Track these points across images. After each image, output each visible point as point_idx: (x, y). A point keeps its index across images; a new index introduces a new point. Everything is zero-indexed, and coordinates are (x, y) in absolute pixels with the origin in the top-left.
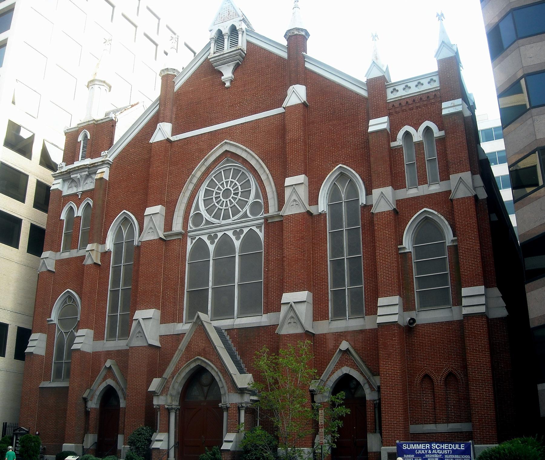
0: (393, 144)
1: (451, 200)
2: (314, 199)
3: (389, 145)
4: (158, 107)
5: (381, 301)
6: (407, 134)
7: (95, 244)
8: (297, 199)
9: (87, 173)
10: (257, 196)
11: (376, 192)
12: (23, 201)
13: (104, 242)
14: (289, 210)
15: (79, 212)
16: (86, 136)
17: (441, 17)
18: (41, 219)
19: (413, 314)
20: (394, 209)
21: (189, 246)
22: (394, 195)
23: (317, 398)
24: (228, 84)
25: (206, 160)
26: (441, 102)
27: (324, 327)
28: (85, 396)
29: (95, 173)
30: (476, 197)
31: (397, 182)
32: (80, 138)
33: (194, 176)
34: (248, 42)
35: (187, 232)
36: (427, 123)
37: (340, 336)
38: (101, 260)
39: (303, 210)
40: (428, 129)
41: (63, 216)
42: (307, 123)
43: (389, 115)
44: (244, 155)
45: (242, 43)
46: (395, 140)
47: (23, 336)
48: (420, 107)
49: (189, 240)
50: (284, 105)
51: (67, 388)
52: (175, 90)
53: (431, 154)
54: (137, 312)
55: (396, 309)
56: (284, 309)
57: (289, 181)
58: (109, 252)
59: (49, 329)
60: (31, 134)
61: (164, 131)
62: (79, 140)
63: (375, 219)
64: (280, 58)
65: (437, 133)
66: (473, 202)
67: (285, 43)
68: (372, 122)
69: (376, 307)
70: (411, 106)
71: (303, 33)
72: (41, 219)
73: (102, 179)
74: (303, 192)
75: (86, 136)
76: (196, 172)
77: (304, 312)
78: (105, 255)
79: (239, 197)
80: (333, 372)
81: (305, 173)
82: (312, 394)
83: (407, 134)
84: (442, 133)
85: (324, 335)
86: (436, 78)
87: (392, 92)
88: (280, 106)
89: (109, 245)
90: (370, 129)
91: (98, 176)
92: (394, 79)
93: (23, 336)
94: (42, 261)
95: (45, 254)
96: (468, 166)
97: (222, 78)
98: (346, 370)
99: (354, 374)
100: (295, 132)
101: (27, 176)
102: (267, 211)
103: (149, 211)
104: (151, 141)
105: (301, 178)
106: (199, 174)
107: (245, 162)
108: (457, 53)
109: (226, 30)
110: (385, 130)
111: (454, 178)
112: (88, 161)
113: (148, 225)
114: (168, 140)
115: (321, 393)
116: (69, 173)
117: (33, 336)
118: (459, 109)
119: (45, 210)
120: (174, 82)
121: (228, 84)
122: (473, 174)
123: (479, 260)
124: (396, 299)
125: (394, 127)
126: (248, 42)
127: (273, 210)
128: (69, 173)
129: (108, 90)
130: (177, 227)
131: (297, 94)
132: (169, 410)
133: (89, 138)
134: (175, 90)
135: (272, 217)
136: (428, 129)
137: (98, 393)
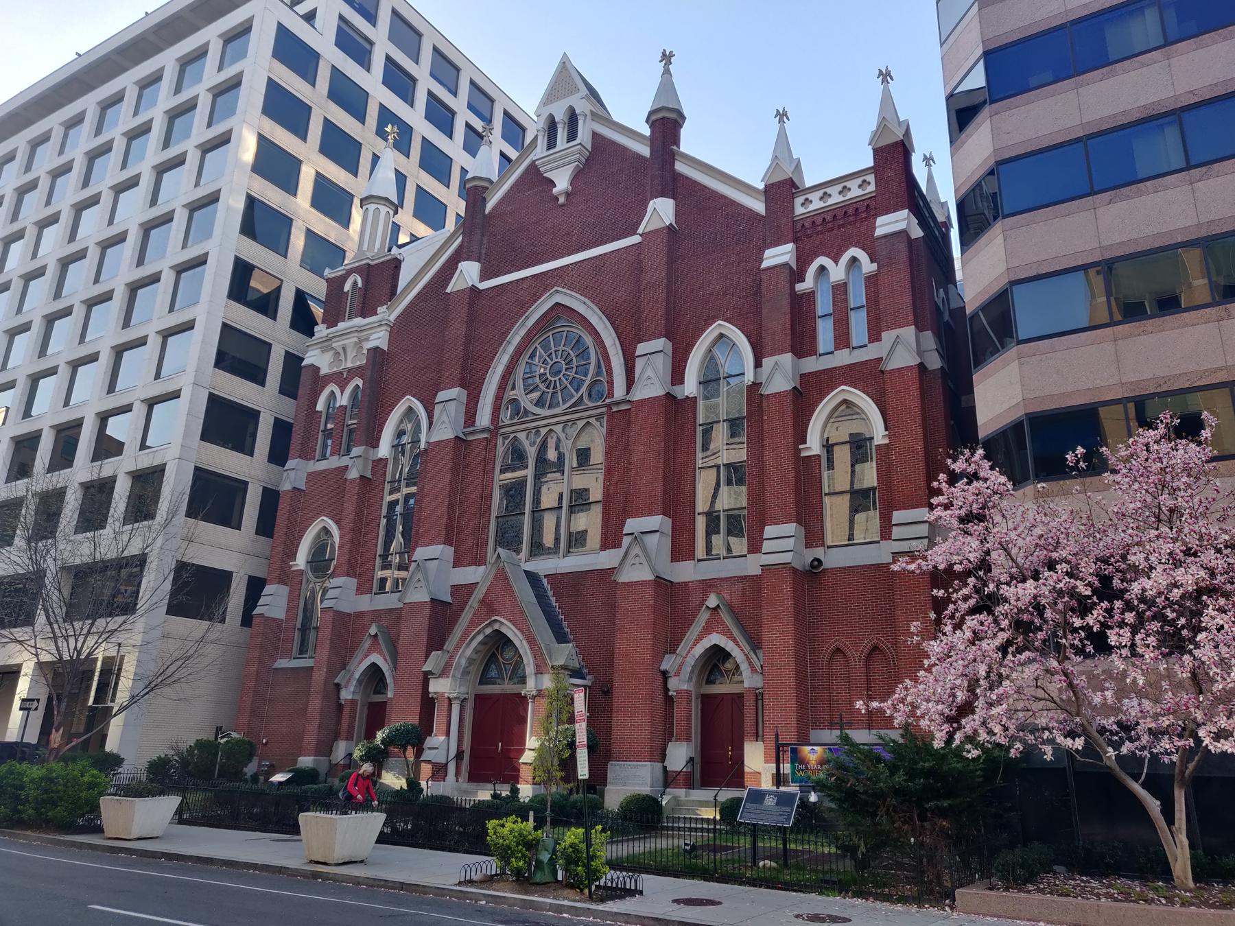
0: (799, 287)
1: (882, 372)
2: (677, 376)
3: (792, 288)
4: (460, 239)
5: (769, 531)
6: (822, 269)
7: (363, 448)
8: (652, 376)
9: (355, 339)
10: (598, 373)
11: (768, 362)
12: (262, 383)
13: (375, 444)
14: (639, 394)
15: (343, 400)
16: (355, 283)
17: (885, 76)
18: (287, 409)
19: (819, 552)
20: (795, 388)
21: (500, 450)
22: (795, 367)
23: (673, 684)
24: (562, 200)
25: (527, 318)
26: (876, 216)
27: (685, 572)
28: (336, 681)
29: (367, 340)
30: (921, 367)
31: (803, 344)
32: (347, 287)
33: (509, 342)
34: (595, 135)
35: (497, 428)
36: (854, 251)
37: (708, 585)
38: (373, 472)
39: (661, 392)
40: (854, 260)
41: (320, 406)
42: (672, 258)
43: (796, 240)
44: (581, 309)
45: (584, 135)
46: (802, 280)
47: (255, 587)
48: (844, 224)
49: (500, 440)
50: (640, 231)
51: (312, 668)
52: (487, 211)
53: (858, 296)
54: (419, 550)
55: (789, 544)
56: (626, 541)
57: (641, 348)
58: (384, 461)
59: (286, 576)
60: (277, 283)
61: (469, 272)
62: (346, 290)
63: (765, 404)
64: (639, 157)
65: (868, 267)
66: (915, 374)
67: (646, 131)
68: (768, 253)
69: (762, 540)
70: (830, 225)
71: (673, 116)
72: (287, 409)
73: (376, 349)
74: (662, 365)
75: (355, 283)
76: (513, 337)
77: (660, 545)
78: (380, 463)
79: (573, 374)
80: (696, 642)
81: (668, 336)
82: (665, 674)
83: (822, 269)
84: (874, 266)
85: (686, 583)
86: (871, 178)
87: (803, 205)
88: (633, 232)
89: (384, 449)
90: (765, 265)
91: (371, 344)
92: (810, 178)
93: (255, 587)
94: (285, 474)
95: (290, 464)
96: (911, 318)
97: (555, 190)
98: (715, 639)
99: (729, 645)
100: (656, 271)
101: (270, 345)
102: (611, 394)
103: (442, 396)
104: (448, 290)
105: (660, 343)
106: (516, 340)
107: (584, 321)
108: (907, 133)
109: (560, 116)
110: (786, 265)
111: (888, 336)
112: (359, 321)
113: (439, 418)
114: (473, 289)
115: (677, 674)
116: (330, 339)
117: (268, 589)
118: (902, 226)
119: (294, 396)
120: (484, 199)
121: (562, 200)
122: (920, 328)
123: (922, 464)
124: (791, 528)
125: (803, 260)
126: (595, 135)
127: (619, 391)
128: (330, 339)
129: (392, 213)
130: (484, 418)
131: (662, 211)
132: (450, 700)
133: (360, 285)
134: (487, 211)
135: (617, 403)
136: (854, 260)
137: (357, 675)
